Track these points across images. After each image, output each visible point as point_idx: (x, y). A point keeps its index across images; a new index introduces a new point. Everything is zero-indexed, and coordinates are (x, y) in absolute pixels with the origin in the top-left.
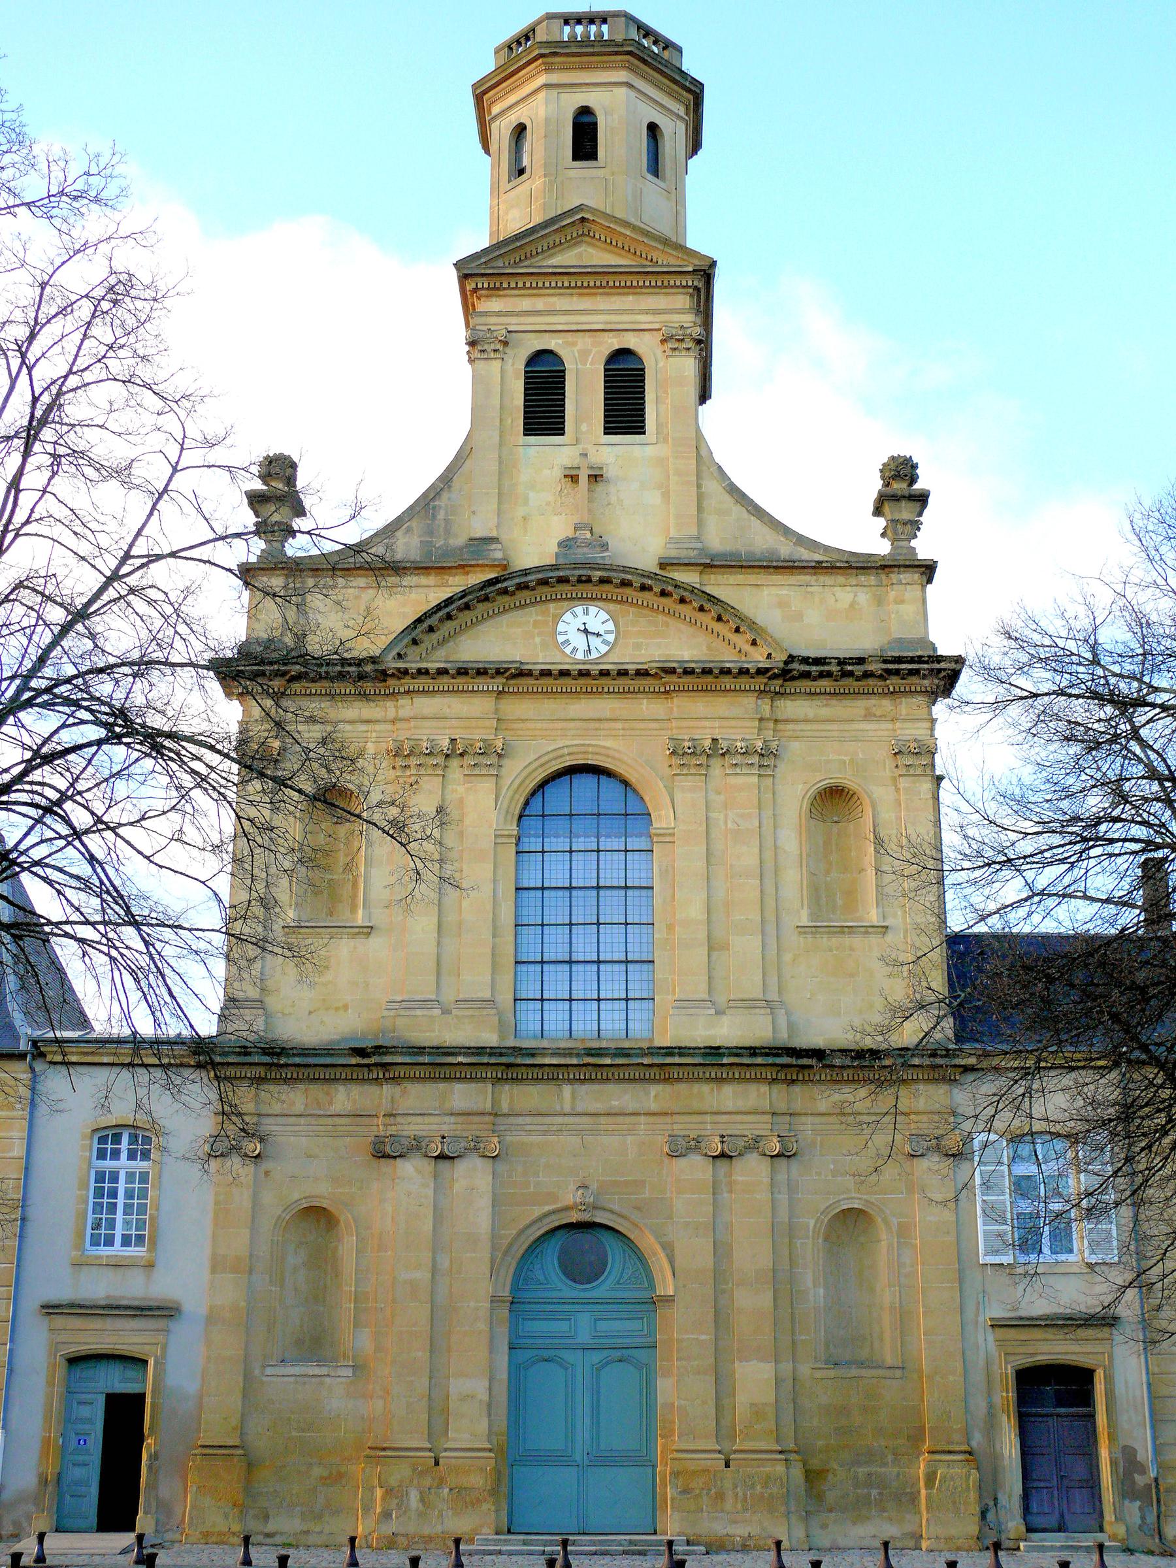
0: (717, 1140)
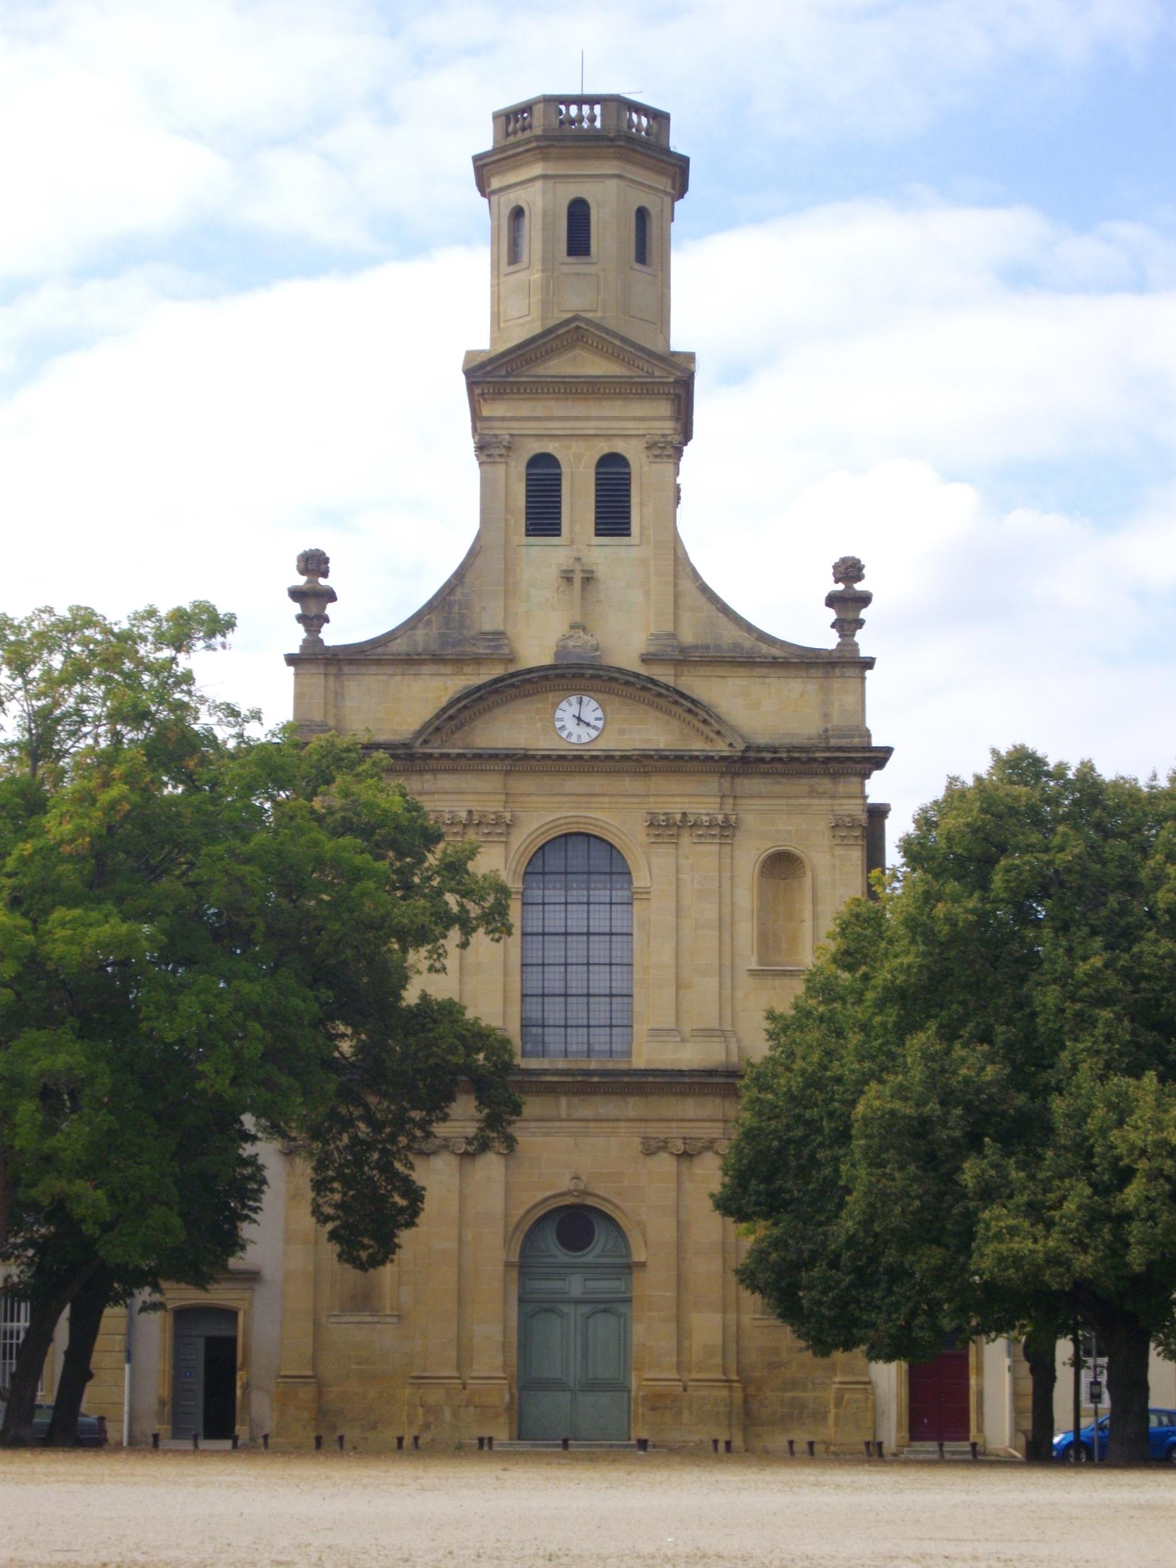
0: (681, 1141)
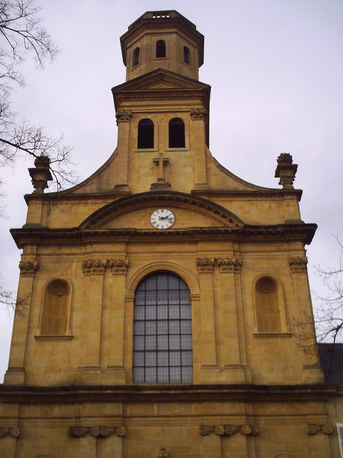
0: (222, 427)
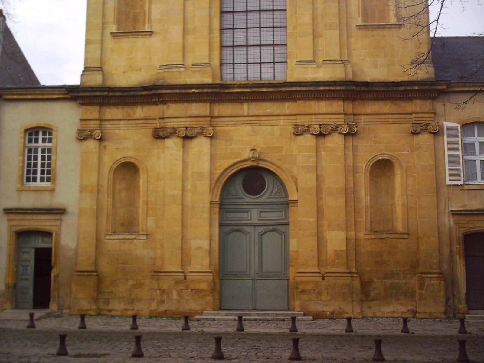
0: (318, 126)
